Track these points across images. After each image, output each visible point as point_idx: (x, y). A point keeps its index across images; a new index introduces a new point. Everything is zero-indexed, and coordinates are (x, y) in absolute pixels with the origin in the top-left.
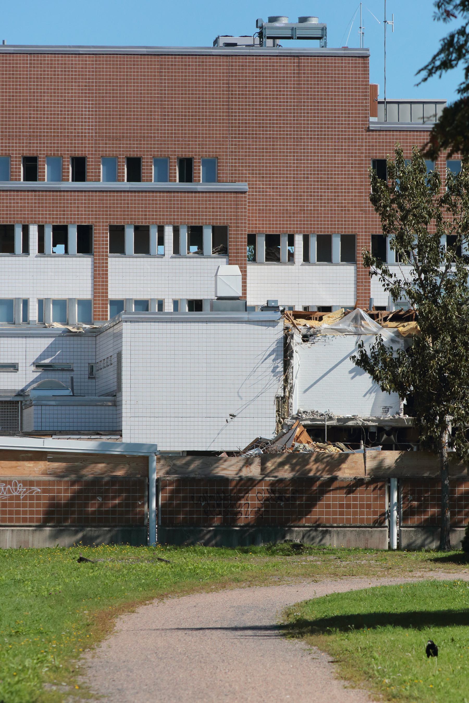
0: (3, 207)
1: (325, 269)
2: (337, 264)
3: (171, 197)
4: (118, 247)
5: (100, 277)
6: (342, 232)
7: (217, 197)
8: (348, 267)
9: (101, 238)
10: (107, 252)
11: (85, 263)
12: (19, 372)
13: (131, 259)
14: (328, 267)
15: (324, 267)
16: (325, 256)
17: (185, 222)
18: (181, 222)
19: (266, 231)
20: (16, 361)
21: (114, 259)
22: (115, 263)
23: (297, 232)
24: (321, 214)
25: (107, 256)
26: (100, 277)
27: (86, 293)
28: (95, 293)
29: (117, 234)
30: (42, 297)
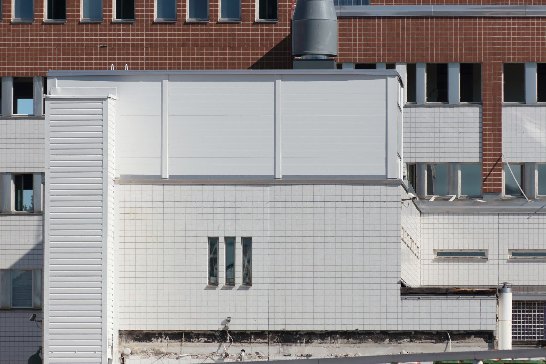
0: (4, 64)
1: (439, 112)
2: (533, 105)
3: (418, 24)
4: (516, 94)
5: (491, 134)
6: (355, 59)
7: (193, 30)
8: (470, 109)
9: (495, 80)
10: (500, 100)
11: (471, 114)
12: (490, 262)
13: (533, 109)
14: (442, 109)
15: (437, 109)
16: (439, 94)
17: (384, 59)
18: (418, 59)
19: (538, 59)
20: (206, 240)
21: (509, 109)
22: (511, 114)
23: (451, 61)
24: (55, 45)
25: (500, 105)
26: (491, 134)
27: (472, 155)
28: (484, 155)
29: (471, 73)
30: (413, 161)
